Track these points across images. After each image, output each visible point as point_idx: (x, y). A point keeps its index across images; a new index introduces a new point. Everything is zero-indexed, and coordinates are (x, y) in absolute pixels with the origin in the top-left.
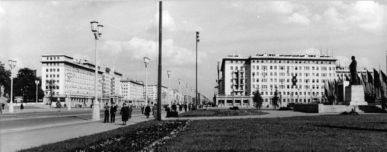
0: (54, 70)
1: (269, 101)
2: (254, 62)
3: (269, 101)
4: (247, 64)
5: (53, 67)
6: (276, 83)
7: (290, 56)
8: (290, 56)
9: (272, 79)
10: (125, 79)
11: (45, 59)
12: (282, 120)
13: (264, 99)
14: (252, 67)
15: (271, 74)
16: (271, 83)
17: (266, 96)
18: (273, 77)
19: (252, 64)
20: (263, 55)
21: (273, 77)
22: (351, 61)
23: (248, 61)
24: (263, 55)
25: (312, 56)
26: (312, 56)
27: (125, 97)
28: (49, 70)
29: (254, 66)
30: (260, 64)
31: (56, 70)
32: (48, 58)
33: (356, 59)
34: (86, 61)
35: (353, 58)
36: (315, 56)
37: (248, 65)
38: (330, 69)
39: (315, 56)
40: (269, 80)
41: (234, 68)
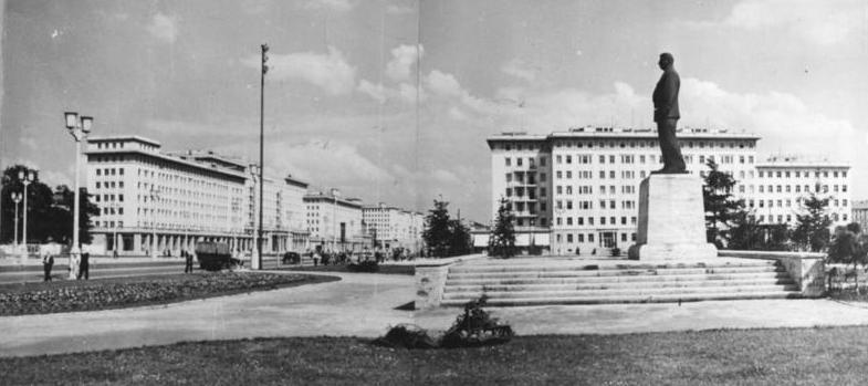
0: (113, 171)
1: (596, 238)
2: (559, 146)
3: (596, 238)
4: (546, 152)
5: (110, 165)
6: (613, 197)
7: (630, 131)
8: (630, 131)
9: (603, 188)
10: (316, 194)
11: (94, 148)
12: (176, 297)
13: (102, 209)
14: (554, 159)
15: (602, 174)
16: (603, 197)
17: (591, 227)
18: (607, 182)
19: (556, 151)
20: (582, 130)
21: (607, 182)
22: (660, 73)
23: (547, 145)
24: (582, 130)
25: (698, 131)
26: (698, 131)
27: (314, 234)
28: (103, 172)
29: (559, 157)
30: (575, 152)
31: (118, 172)
32: (100, 146)
33: (677, 67)
34: (211, 153)
35: (666, 61)
36: (705, 131)
37: (546, 155)
38: (742, 161)
39: (705, 131)
40: (596, 189)
41: (514, 162)
